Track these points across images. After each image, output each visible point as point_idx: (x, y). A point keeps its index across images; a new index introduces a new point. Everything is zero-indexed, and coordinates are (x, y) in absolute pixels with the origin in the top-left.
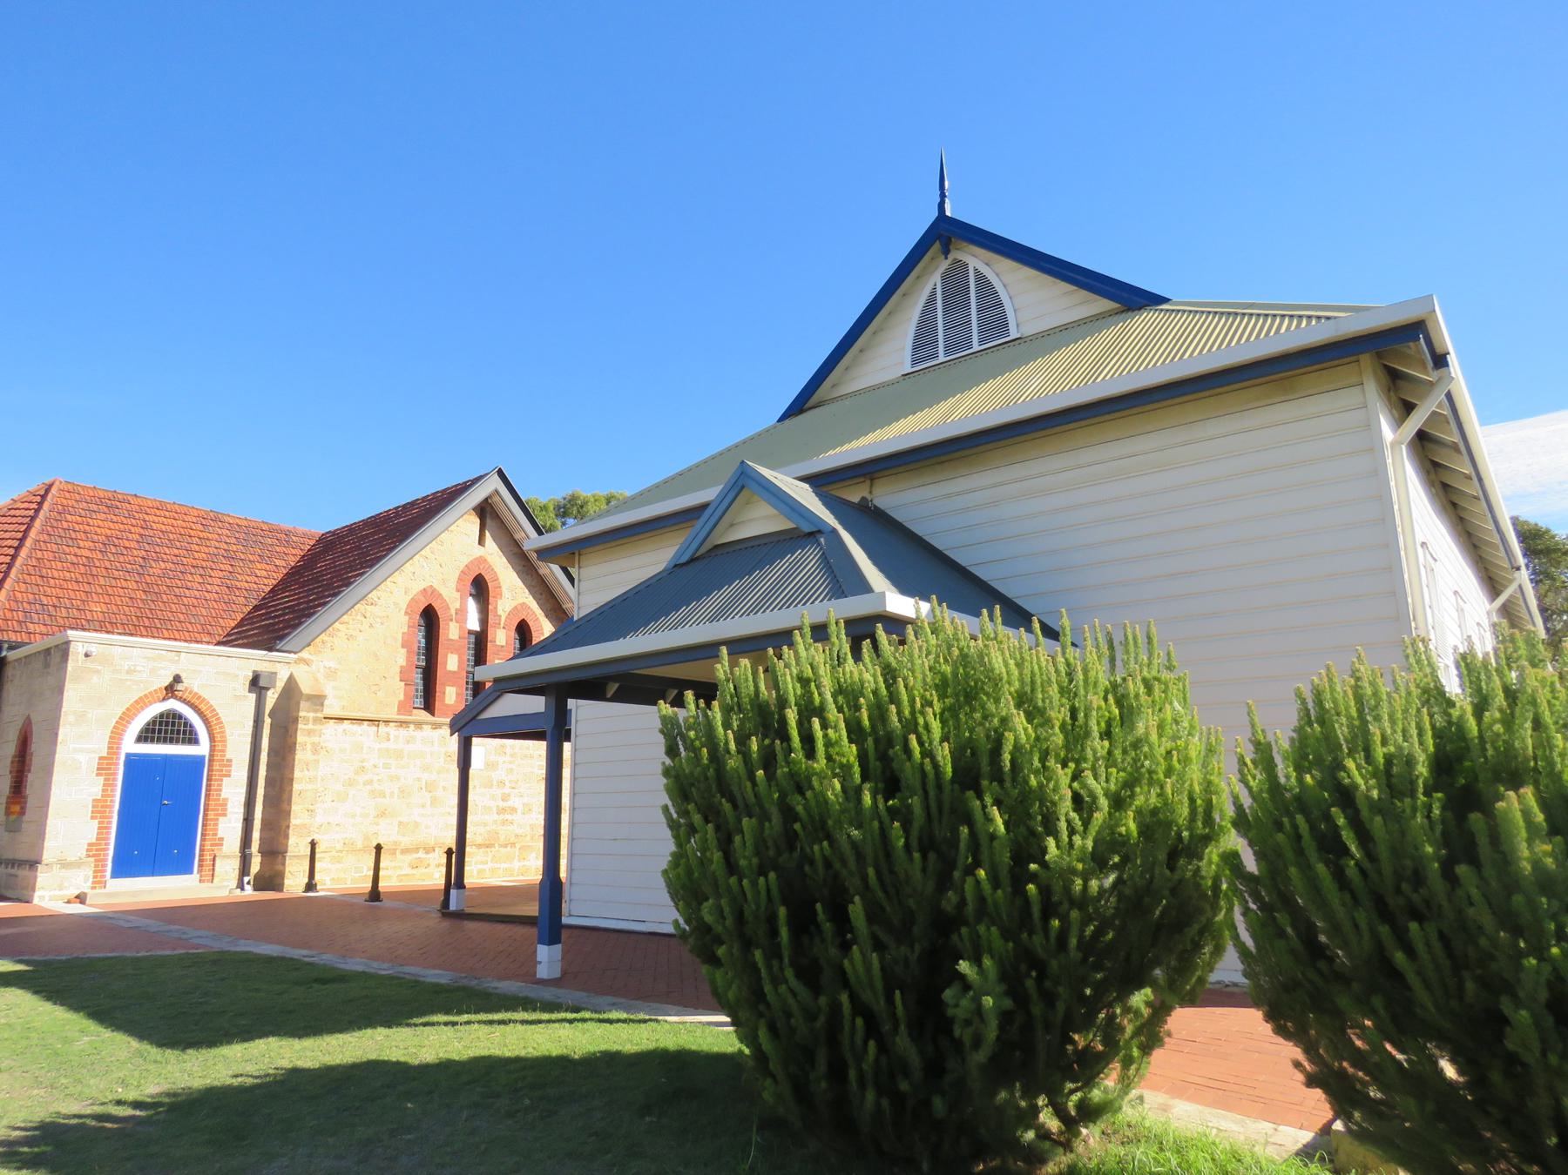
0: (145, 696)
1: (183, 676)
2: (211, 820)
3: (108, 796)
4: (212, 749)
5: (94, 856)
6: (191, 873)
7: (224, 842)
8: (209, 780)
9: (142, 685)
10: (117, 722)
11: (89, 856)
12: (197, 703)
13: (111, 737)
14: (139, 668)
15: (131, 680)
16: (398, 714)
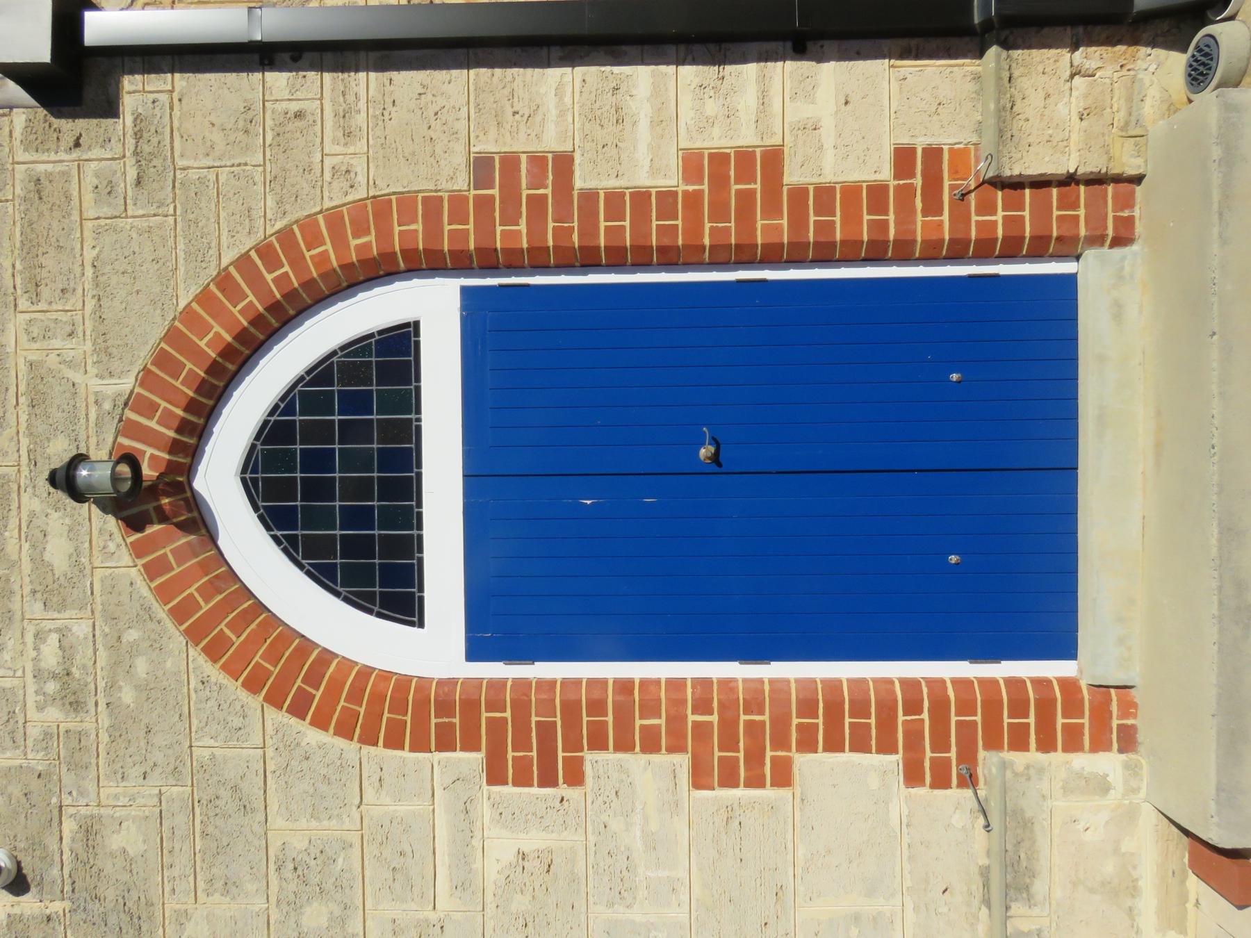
0: (179, 614)
1: (59, 452)
2: (798, 220)
3: (676, 721)
4: (446, 191)
5: (968, 756)
7: (921, 142)
8: (589, 261)
9: (132, 635)
10: (320, 723)
11: (969, 780)
12: (239, 314)
13: (394, 742)
14: (50, 656)
15: (112, 686)
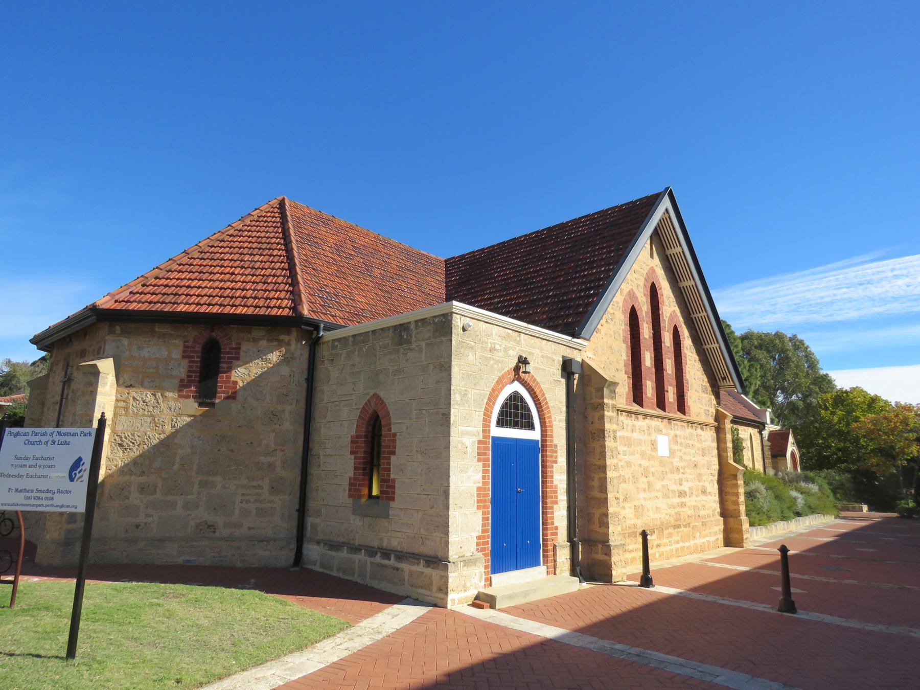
6: (540, 565)
16: (627, 404)
